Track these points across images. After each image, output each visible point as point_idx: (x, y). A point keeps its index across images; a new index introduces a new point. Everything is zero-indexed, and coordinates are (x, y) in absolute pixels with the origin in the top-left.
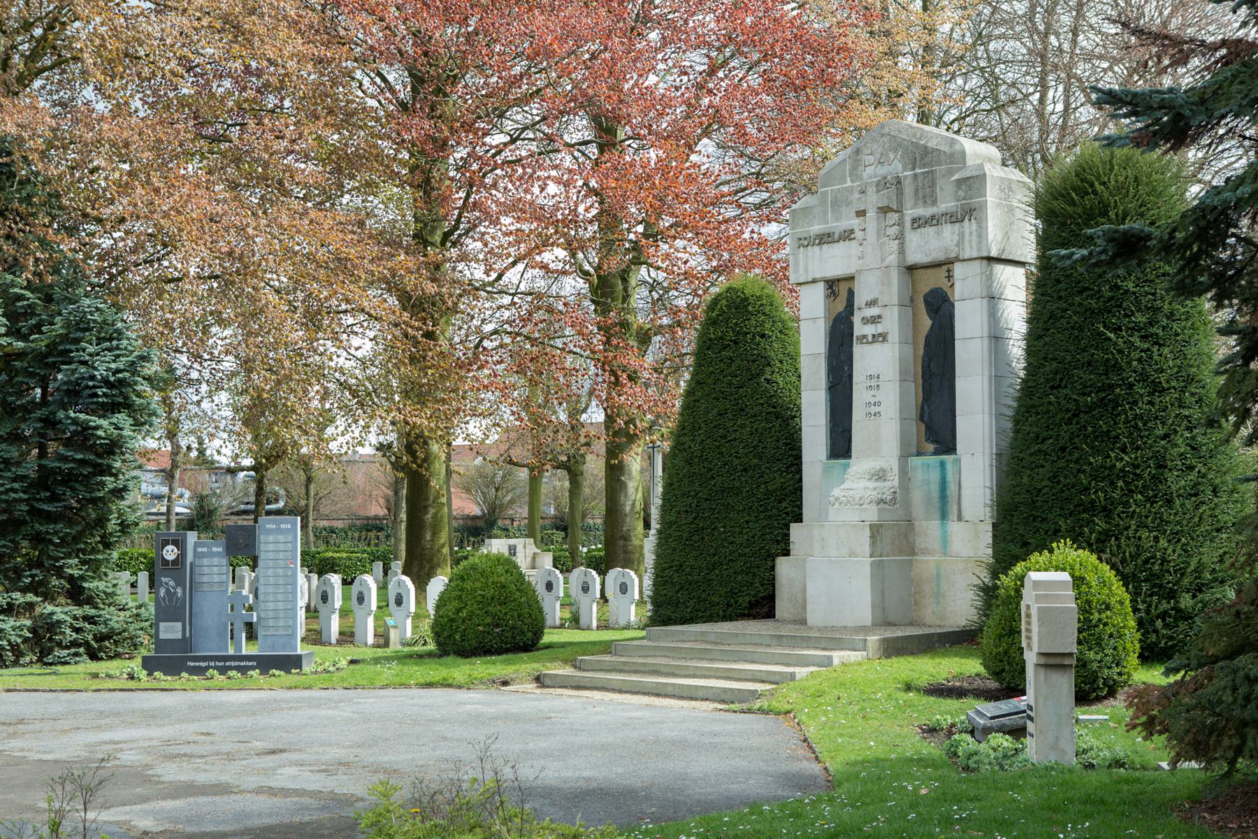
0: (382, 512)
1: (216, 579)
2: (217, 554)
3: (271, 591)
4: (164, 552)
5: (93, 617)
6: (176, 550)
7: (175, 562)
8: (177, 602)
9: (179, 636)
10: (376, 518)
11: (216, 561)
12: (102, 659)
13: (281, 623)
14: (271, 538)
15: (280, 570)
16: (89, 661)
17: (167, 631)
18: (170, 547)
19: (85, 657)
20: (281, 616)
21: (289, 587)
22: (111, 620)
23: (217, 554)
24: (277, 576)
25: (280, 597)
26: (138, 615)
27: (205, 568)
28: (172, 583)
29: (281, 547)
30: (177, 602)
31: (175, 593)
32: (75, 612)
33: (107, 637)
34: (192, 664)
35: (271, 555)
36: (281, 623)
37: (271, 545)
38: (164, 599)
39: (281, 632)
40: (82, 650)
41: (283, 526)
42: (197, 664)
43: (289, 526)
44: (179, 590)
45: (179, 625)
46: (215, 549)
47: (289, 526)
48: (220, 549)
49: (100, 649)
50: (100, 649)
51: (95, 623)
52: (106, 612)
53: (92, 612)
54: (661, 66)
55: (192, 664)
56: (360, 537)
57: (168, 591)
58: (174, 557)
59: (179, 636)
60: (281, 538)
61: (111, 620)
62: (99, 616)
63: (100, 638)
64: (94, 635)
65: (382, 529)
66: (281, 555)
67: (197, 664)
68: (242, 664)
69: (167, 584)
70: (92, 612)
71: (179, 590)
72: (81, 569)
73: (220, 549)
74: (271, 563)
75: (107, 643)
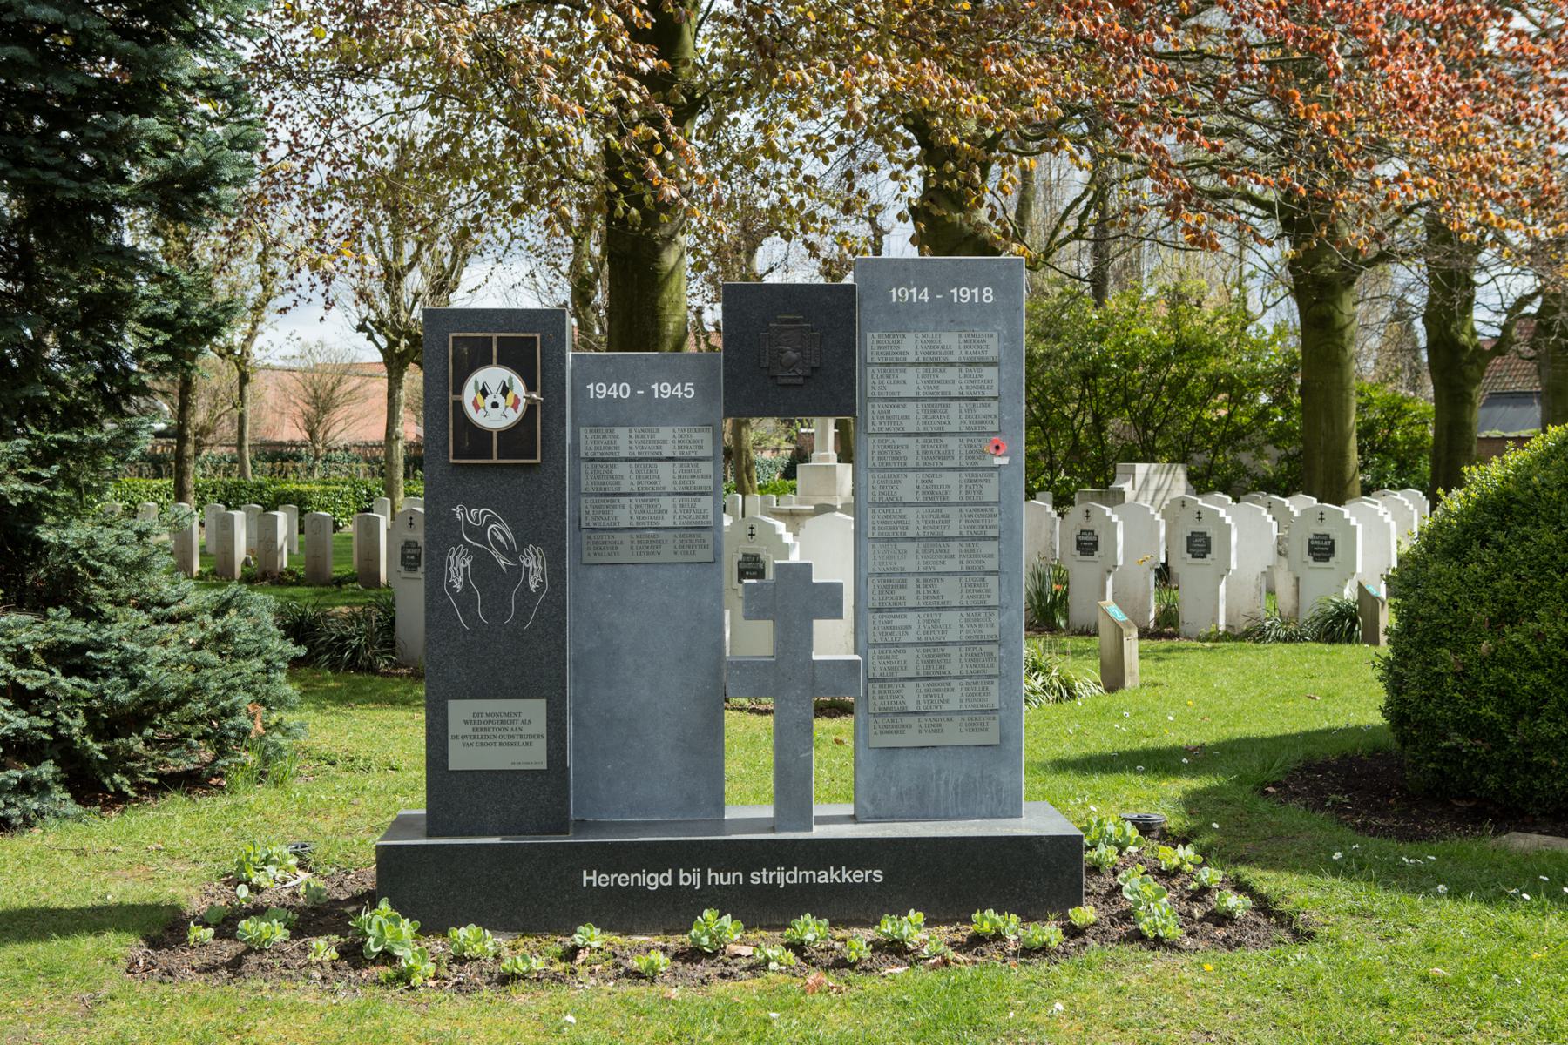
0: (300, 436)
1: (670, 512)
2: (673, 411)
3: (911, 563)
4: (469, 394)
5: (80, 649)
6: (519, 388)
7: (517, 438)
8: (524, 611)
9: (535, 756)
10: (293, 444)
11: (668, 437)
12: (121, 797)
13: (955, 699)
14: (911, 345)
15: (951, 479)
16: (72, 808)
17: (481, 733)
18: (493, 375)
19: (58, 793)
20: (954, 668)
21: (989, 548)
22: (143, 658)
23: (673, 411)
24: (935, 502)
25: (951, 591)
26: (223, 637)
27: (622, 469)
28: (501, 531)
29: (954, 381)
30: (524, 611)
31: (518, 572)
32: (24, 636)
33: (135, 719)
34: (602, 880)
35: (912, 416)
36: (955, 699)
37: (911, 374)
38: (466, 599)
39: (953, 734)
40: (47, 770)
41: (962, 295)
42: (625, 880)
43: (988, 295)
44: (533, 563)
45: (534, 712)
46: (664, 390)
47: (988, 295)
48: (685, 391)
49: (119, 761)
50: (119, 761)
51: (86, 670)
52: (125, 626)
53: (79, 631)
54: (434, 28)
55: (602, 880)
56: (273, 469)
57: (482, 563)
58: (513, 417)
59: (535, 756)
60: (952, 343)
61: (143, 658)
62: (100, 647)
63: (111, 723)
64: (90, 713)
65: (299, 459)
66: (955, 417)
67: (625, 880)
68: (825, 877)
69: (478, 533)
70: (79, 631)
71: (533, 563)
72: (33, 478)
73: (685, 391)
74: (911, 451)
75: (136, 743)
